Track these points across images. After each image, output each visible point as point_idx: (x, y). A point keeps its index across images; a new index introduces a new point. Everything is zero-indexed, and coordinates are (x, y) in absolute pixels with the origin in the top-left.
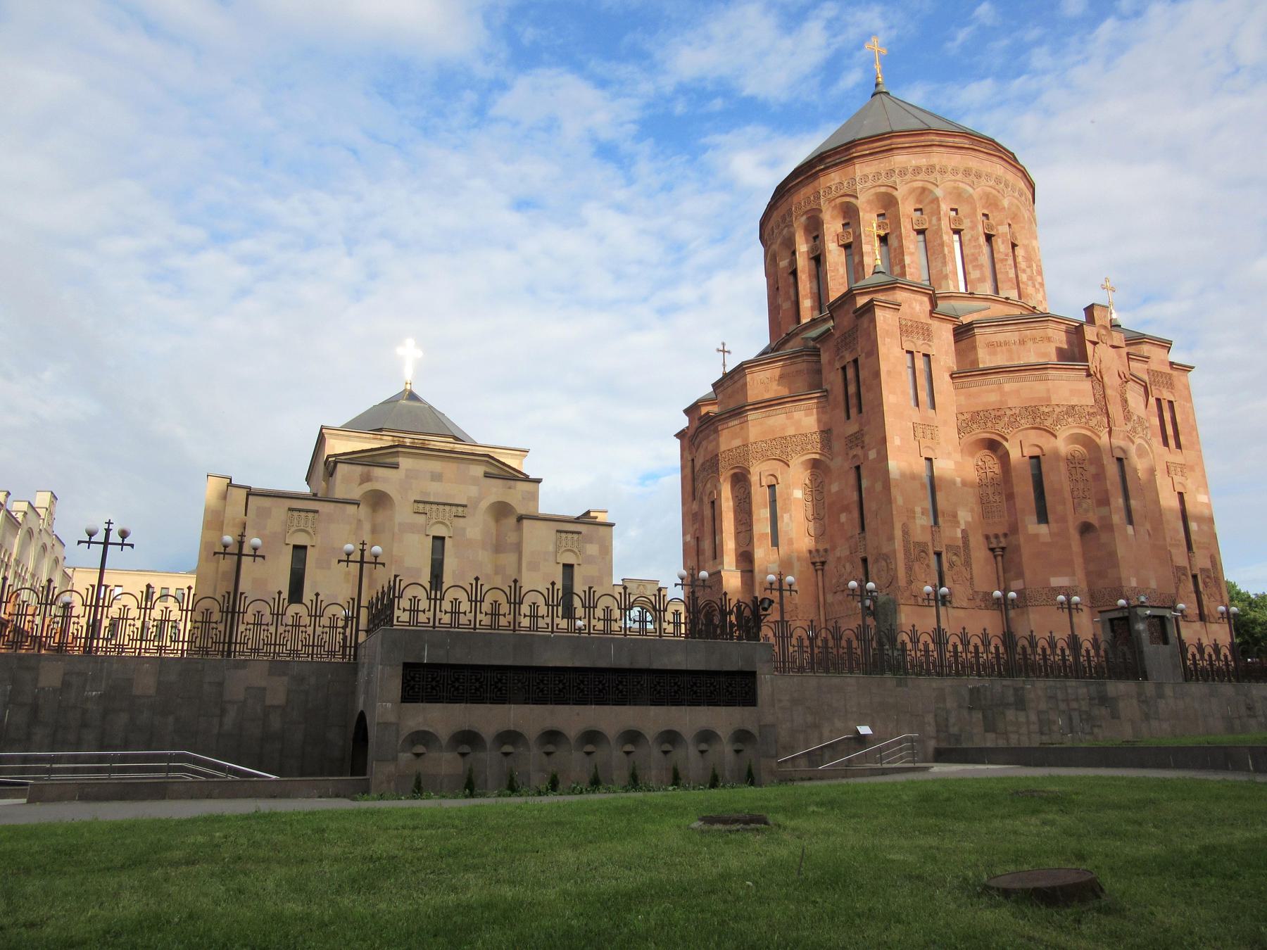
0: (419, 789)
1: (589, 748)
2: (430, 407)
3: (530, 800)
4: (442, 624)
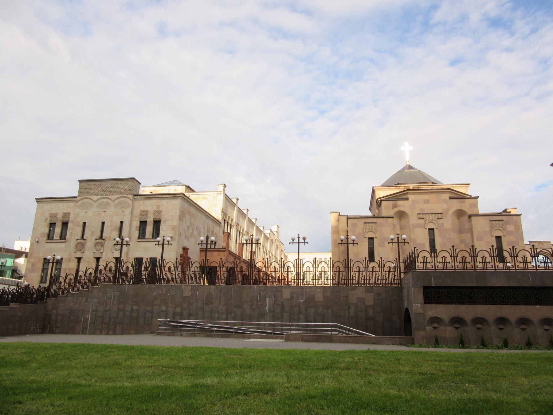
0: (437, 343)
1: (523, 327)
2: (419, 171)
3: (495, 351)
4: (419, 268)
